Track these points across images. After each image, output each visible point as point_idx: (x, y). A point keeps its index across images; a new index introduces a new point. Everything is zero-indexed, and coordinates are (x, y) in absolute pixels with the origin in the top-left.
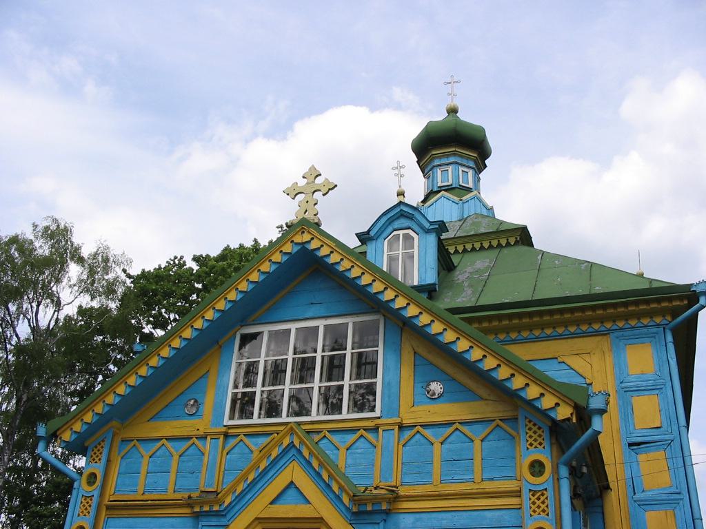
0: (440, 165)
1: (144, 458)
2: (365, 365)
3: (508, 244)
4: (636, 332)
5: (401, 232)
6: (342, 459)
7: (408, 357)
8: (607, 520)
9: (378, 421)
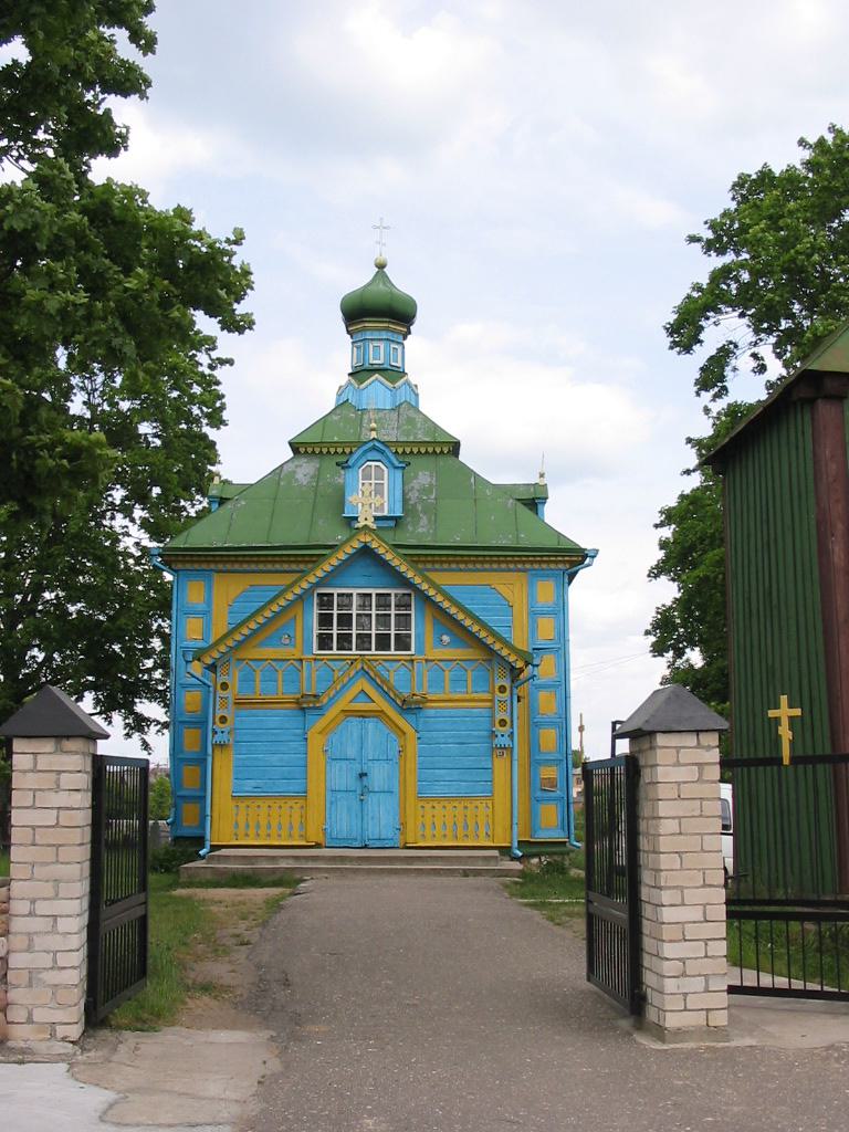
2: (404, 621)
3: (442, 452)
5: (373, 464)
6: (393, 679)
8: (823, 1016)
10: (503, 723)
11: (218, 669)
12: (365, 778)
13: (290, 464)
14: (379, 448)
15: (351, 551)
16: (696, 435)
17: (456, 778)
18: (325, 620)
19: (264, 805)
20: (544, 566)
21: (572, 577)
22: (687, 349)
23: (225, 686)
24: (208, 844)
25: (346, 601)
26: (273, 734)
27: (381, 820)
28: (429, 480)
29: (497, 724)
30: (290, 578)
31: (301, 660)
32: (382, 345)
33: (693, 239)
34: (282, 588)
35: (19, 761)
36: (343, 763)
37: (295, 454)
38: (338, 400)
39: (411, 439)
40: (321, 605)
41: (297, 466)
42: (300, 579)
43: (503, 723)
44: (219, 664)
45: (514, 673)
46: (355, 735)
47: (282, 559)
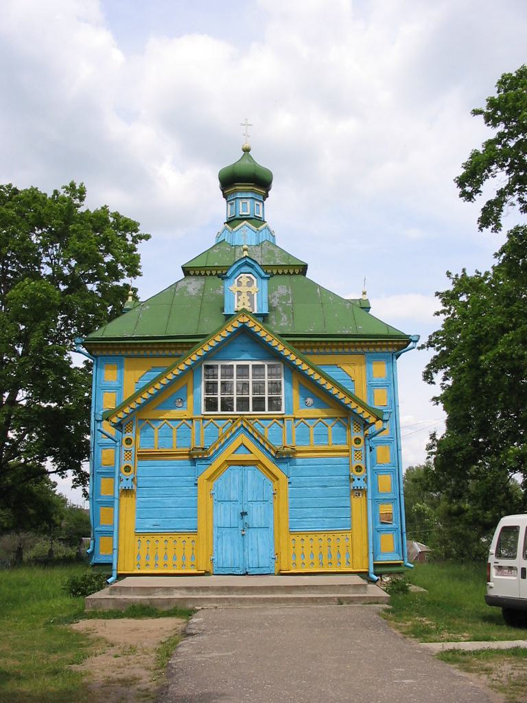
0: (241, 198)
1: (156, 431)
2: (275, 388)
3: (294, 273)
4: (379, 354)
6: (267, 434)
7: (296, 384)
9: (284, 416)
11: (124, 428)
12: (245, 517)
13: (183, 282)
14: (248, 263)
15: (232, 330)
16: (442, 290)
17: (321, 515)
18: (211, 387)
19: (162, 539)
20: (378, 350)
22: (469, 197)
23: (129, 441)
24: (115, 574)
26: (168, 481)
27: (259, 551)
28: (286, 291)
29: (354, 469)
31: (192, 419)
32: (249, 202)
33: (476, 112)
36: (227, 504)
37: (185, 275)
39: (272, 263)
41: (188, 284)
43: (359, 469)
46: (184, 525)
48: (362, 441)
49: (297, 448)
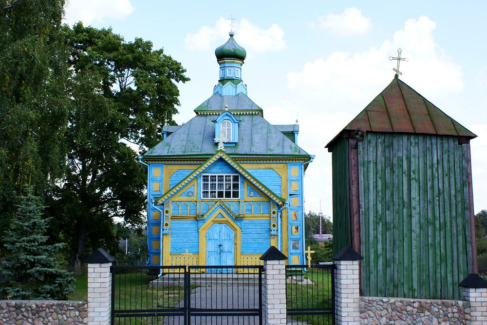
2: (236, 186)
5: (226, 121)
6: (232, 209)
10: (274, 226)
12: (221, 247)
18: (205, 186)
21: (306, 167)
25: (214, 179)
29: (272, 226)
30: (194, 167)
31: (196, 201)
34: (193, 171)
35: (90, 270)
38: (214, 92)
40: (204, 180)
42: (200, 167)
43: (274, 226)
44: (165, 203)
45: (279, 206)
47: (193, 160)
48: (276, 213)
49: (245, 216)
